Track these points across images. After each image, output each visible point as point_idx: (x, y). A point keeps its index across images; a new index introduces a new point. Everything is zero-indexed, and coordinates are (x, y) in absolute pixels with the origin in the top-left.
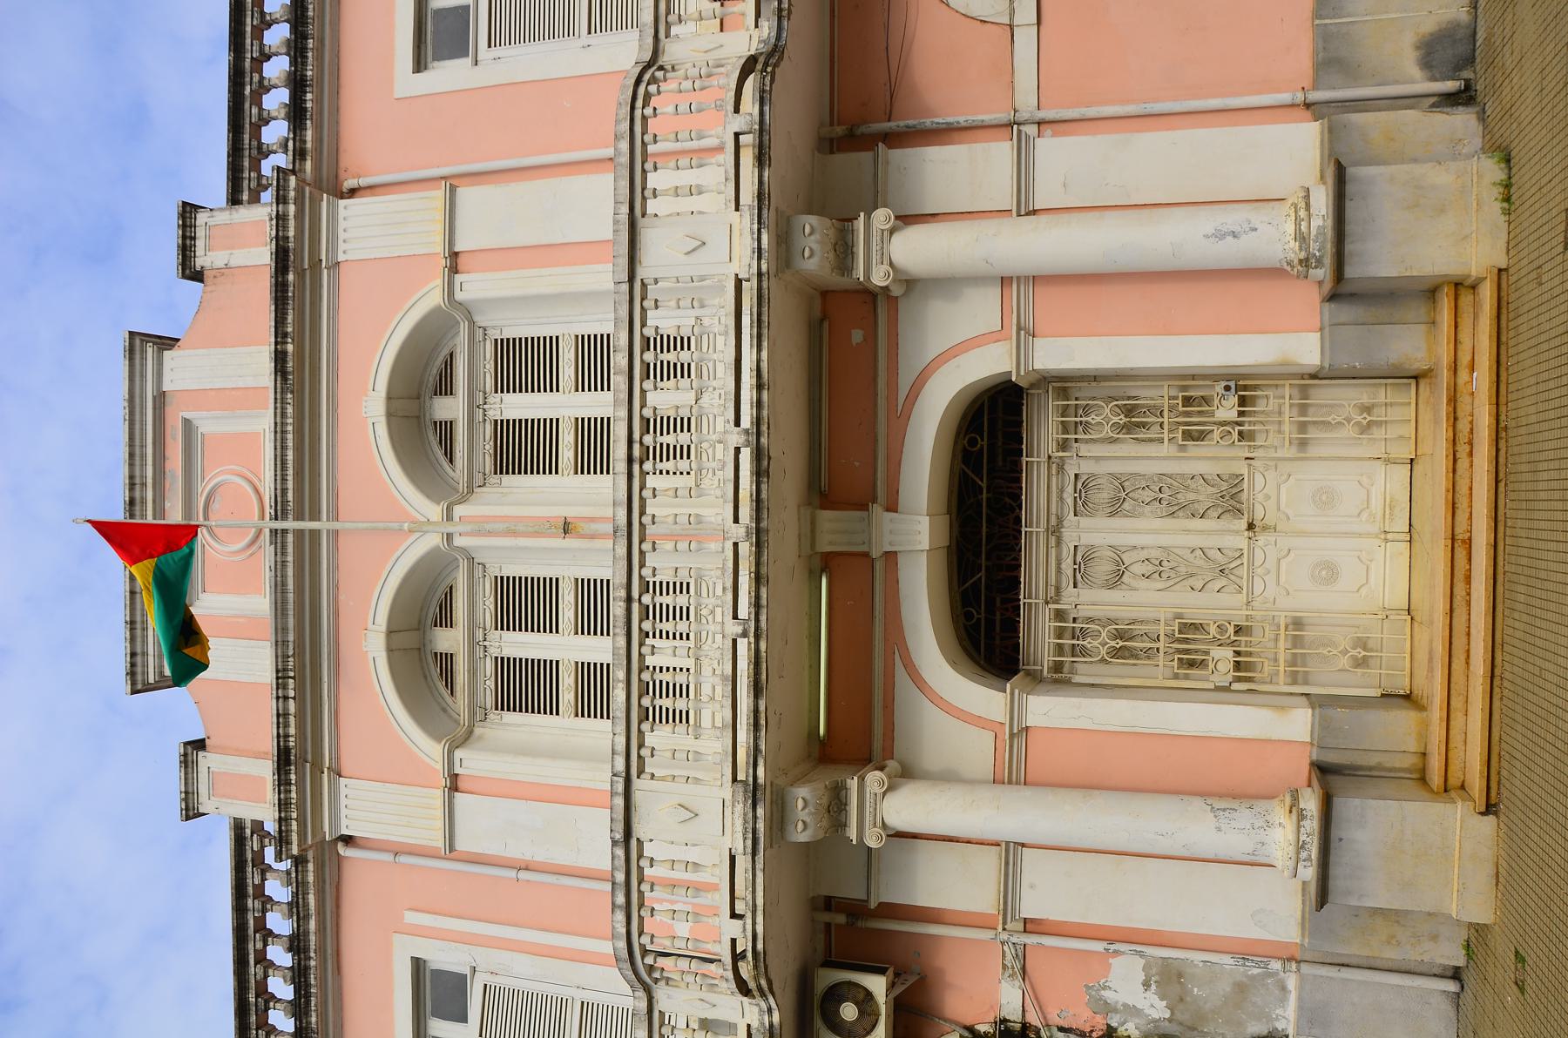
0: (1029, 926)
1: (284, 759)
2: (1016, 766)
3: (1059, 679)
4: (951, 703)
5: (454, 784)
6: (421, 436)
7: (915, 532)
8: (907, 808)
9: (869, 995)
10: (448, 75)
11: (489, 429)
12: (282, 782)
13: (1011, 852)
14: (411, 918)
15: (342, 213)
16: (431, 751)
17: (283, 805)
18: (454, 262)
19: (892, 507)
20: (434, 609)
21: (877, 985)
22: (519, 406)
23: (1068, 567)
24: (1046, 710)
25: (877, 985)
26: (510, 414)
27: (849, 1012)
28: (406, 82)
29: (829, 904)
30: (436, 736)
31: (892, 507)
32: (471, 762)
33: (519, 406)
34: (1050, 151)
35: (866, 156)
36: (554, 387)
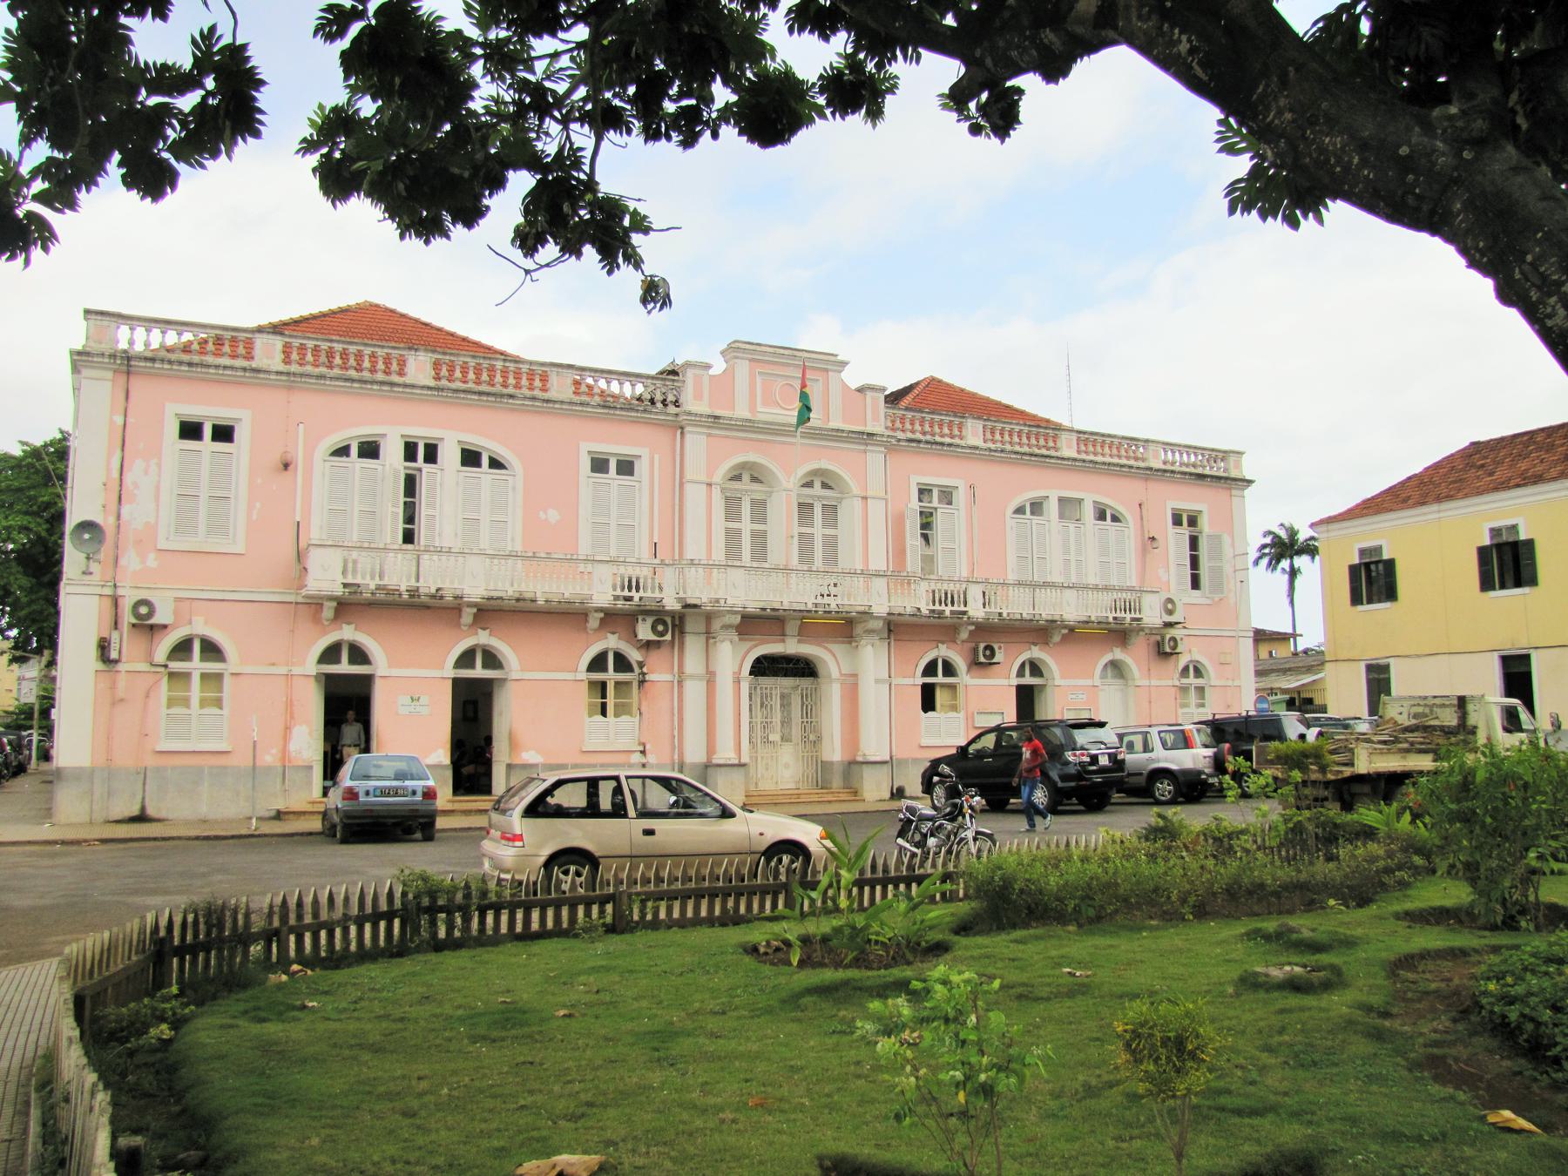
0: (680, 683)
10: (586, 464)
18: (865, 498)
21: (668, 637)
22: (818, 510)
33: (818, 510)
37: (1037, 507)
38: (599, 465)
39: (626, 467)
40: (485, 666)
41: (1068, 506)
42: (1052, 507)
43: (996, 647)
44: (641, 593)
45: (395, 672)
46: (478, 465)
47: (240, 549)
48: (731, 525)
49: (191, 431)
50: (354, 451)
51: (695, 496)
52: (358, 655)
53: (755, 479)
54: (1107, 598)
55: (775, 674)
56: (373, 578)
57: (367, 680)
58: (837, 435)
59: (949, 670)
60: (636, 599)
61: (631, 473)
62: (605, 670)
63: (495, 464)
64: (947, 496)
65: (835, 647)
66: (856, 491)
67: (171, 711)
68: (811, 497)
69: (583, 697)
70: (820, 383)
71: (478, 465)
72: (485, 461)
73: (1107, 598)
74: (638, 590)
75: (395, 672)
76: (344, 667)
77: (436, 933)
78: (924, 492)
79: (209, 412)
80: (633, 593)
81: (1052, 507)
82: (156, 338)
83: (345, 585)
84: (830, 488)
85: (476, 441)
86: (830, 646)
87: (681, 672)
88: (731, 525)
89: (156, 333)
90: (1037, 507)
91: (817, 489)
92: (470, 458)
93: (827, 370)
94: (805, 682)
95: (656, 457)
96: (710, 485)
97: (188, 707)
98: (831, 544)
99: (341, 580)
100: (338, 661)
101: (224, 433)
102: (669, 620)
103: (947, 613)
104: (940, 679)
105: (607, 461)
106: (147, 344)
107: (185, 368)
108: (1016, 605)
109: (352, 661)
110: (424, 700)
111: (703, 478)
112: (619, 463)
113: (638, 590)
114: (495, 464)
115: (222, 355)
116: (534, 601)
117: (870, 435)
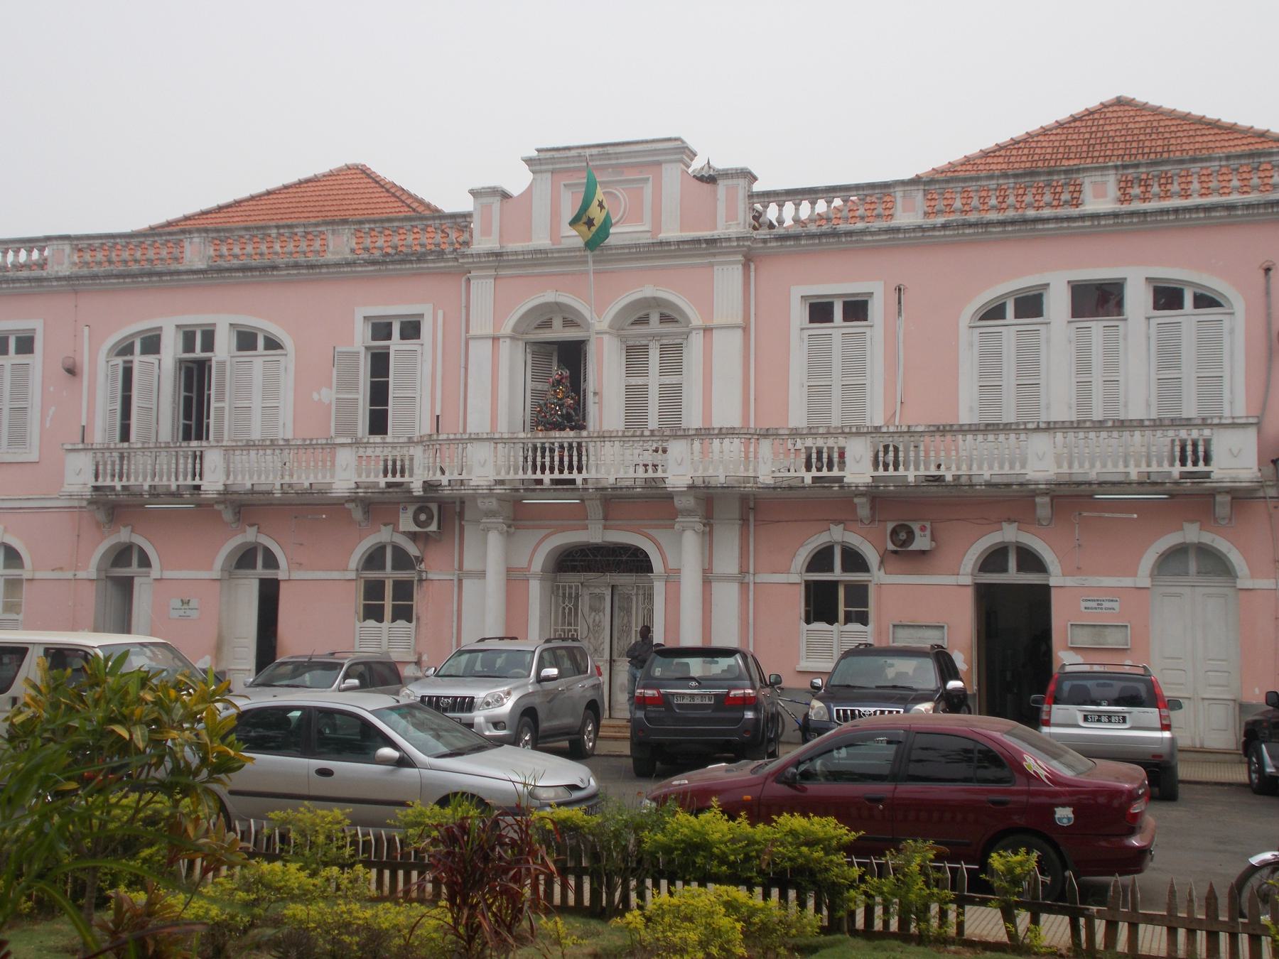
0: (460, 581)
1: (498, 255)
2: (514, 578)
3: (555, 590)
4: (538, 550)
5: (495, 339)
6: (639, 314)
7: (595, 534)
8: (495, 541)
9: (429, 525)
10: (799, 314)
11: (644, 343)
12: (489, 254)
13: (482, 574)
14: (440, 313)
15: (735, 267)
16: (507, 328)
17: (479, 255)
18: (707, 330)
19: (605, 527)
20: (570, 317)
21: (433, 527)
22: (654, 355)
23: (597, 591)
24: (535, 587)
25: (433, 527)
26: (651, 352)
27: (423, 517)
28: (797, 292)
29: (463, 503)
30: (514, 330)
31: (605, 527)
32: (505, 346)
33: (654, 355)
34: (734, 588)
35: (737, 515)
36: (662, 373)
37: (1030, 305)
38: (820, 312)
39: (857, 309)
40: (1021, 568)
41: (1099, 299)
42: (1058, 303)
43: (916, 527)
44: (584, 474)
45: (1069, 581)
46: (1179, 305)
47: (34, 457)
48: (633, 381)
49: (820, 312)
50: (1010, 310)
51: (480, 352)
52: (1030, 561)
53: (665, 319)
54: (1163, 441)
55: (588, 568)
56: (808, 468)
57: (1043, 593)
58: (659, 250)
59: (854, 561)
60: (579, 482)
61: (864, 317)
62: (383, 567)
63: (1205, 301)
64: (412, 329)
65: (658, 534)
66: (696, 320)
67: (395, 625)
68: (645, 336)
69: (355, 599)
70: (650, 184)
71: (1179, 305)
72: (261, 342)
73: (1163, 441)
74: (580, 471)
75: (295, 575)
76: (1013, 576)
77: (419, 875)
78: (381, 329)
79: (836, 287)
80: (575, 475)
81: (1137, 298)
82: (805, 210)
83: (96, 488)
84: (674, 321)
85: (1170, 273)
86: (652, 532)
87: (461, 568)
88: (633, 381)
89: (789, 208)
90: (1030, 305)
91: (655, 325)
92: (1167, 297)
93: (659, 164)
94: (625, 580)
95: (440, 313)
96: (495, 339)
97: (865, 623)
98: (672, 396)
99: (92, 482)
100: (830, 569)
101: (857, 309)
102: (434, 508)
103: (119, 488)
104: (133, 570)
105: (831, 305)
106: (797, 220)
107: (1172, 217)
108: (978, 461)
109: (1021, 568)
110: (194, 603)
111: (489, 331)
112: (19, 340)
113: (580, 471)
114: (1205, 301)
115: (1150, 199)
116: (270, 493)
117: (712, 242)
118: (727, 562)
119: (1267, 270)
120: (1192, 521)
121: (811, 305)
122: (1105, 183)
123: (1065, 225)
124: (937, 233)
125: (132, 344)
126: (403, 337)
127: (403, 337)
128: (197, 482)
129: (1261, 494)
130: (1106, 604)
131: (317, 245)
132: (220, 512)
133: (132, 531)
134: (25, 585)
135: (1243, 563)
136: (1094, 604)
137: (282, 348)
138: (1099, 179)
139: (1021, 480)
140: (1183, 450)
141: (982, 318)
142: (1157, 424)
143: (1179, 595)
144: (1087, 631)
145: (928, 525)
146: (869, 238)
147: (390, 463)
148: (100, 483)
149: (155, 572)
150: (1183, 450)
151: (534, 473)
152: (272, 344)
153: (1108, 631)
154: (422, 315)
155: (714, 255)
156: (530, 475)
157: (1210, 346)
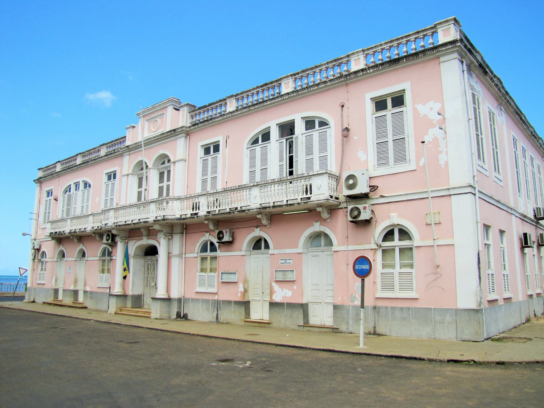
10: (370, 107)
19: (148, 239)
38: (380, 104)
49: (380, 104)
90: (266, 136)
118: (176, 250)
119: (343, 106)
120: (317, 222)
121: (376, 103)
122: (288, 83)
123: (273, 101)
124: (235, 114)
125: (258, 139)
126: (394, 106)
127: (394, 106)
128: (309, 195)
129: (341, 207)
130: (288, 261)
131: (223, 109)
132: (320, 212)
133: (260, 230)
134: (414, 250)
135: (272, 243)
136: (284, 261)
137: (327, 125)
138: (356, 58)
139: (248, 208)
140: (307, 188)
141: (252, 144)
142: (186, 198)
143: (317, 256)
144: (281, 273)
145: (228, 230)
146: (217, 120)
147: (195, 205)
148: (210, 210)
149: (271, 251)
150: (307, 188)
151: (307, 194)
152: (323, 124)
153: (288, 273)
154: (219, 141)
155: (177, 135)
156: (305, 196)
157: (323, 141)
